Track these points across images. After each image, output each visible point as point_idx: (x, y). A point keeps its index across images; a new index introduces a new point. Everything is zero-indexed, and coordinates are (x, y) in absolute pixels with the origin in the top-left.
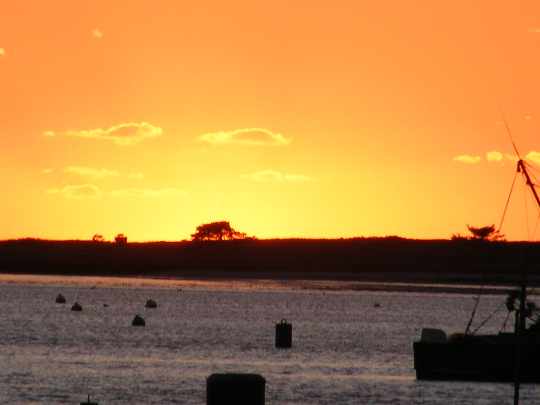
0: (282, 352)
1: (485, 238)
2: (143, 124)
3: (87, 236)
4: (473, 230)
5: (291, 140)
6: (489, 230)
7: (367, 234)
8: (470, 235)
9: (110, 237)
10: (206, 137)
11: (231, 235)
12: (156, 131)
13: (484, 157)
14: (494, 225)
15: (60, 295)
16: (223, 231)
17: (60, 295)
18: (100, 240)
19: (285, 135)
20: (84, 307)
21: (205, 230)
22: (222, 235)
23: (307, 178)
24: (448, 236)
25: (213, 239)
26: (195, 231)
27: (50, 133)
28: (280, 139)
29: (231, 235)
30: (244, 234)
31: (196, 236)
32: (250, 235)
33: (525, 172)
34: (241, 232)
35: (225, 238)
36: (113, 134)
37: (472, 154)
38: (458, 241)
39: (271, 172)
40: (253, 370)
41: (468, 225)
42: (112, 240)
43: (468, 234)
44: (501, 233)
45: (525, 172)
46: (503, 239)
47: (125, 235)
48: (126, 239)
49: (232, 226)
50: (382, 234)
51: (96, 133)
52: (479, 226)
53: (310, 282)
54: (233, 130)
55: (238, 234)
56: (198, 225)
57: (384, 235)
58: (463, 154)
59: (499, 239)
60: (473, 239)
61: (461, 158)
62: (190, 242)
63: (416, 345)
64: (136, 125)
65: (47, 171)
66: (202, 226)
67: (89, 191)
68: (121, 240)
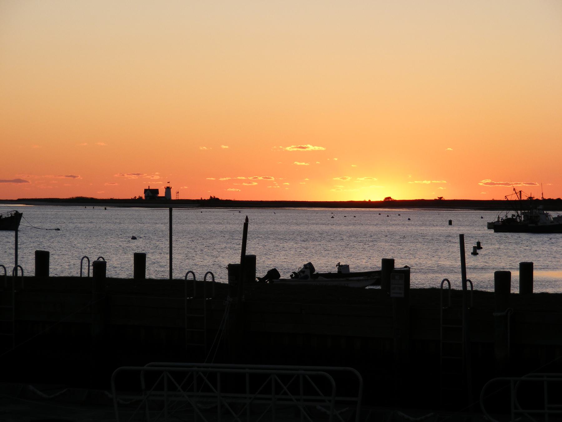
0: (450, 226)
6: (442, 198)
7: (418, 199)
8: (438, 199)
9: (367, 200)
10: (358, 179)
12: (349, 178)
14: (201, 198)
15: (488, 223)
17: (488, 223)
21: (386, 198)
24: (433, 199)
28: (375, 179)
33: (515, 191)
35: (390, 200)
36: (365, 179)
38: (435, 200)
40: (556, 236)
45: (515, 191)
51: (338, 179)
53: (415, 209)
57: (414, 199)
62: (367, 202)
63: (244, 223)
65: (145, 183)
66: (71, 198)
68: (370, 201)
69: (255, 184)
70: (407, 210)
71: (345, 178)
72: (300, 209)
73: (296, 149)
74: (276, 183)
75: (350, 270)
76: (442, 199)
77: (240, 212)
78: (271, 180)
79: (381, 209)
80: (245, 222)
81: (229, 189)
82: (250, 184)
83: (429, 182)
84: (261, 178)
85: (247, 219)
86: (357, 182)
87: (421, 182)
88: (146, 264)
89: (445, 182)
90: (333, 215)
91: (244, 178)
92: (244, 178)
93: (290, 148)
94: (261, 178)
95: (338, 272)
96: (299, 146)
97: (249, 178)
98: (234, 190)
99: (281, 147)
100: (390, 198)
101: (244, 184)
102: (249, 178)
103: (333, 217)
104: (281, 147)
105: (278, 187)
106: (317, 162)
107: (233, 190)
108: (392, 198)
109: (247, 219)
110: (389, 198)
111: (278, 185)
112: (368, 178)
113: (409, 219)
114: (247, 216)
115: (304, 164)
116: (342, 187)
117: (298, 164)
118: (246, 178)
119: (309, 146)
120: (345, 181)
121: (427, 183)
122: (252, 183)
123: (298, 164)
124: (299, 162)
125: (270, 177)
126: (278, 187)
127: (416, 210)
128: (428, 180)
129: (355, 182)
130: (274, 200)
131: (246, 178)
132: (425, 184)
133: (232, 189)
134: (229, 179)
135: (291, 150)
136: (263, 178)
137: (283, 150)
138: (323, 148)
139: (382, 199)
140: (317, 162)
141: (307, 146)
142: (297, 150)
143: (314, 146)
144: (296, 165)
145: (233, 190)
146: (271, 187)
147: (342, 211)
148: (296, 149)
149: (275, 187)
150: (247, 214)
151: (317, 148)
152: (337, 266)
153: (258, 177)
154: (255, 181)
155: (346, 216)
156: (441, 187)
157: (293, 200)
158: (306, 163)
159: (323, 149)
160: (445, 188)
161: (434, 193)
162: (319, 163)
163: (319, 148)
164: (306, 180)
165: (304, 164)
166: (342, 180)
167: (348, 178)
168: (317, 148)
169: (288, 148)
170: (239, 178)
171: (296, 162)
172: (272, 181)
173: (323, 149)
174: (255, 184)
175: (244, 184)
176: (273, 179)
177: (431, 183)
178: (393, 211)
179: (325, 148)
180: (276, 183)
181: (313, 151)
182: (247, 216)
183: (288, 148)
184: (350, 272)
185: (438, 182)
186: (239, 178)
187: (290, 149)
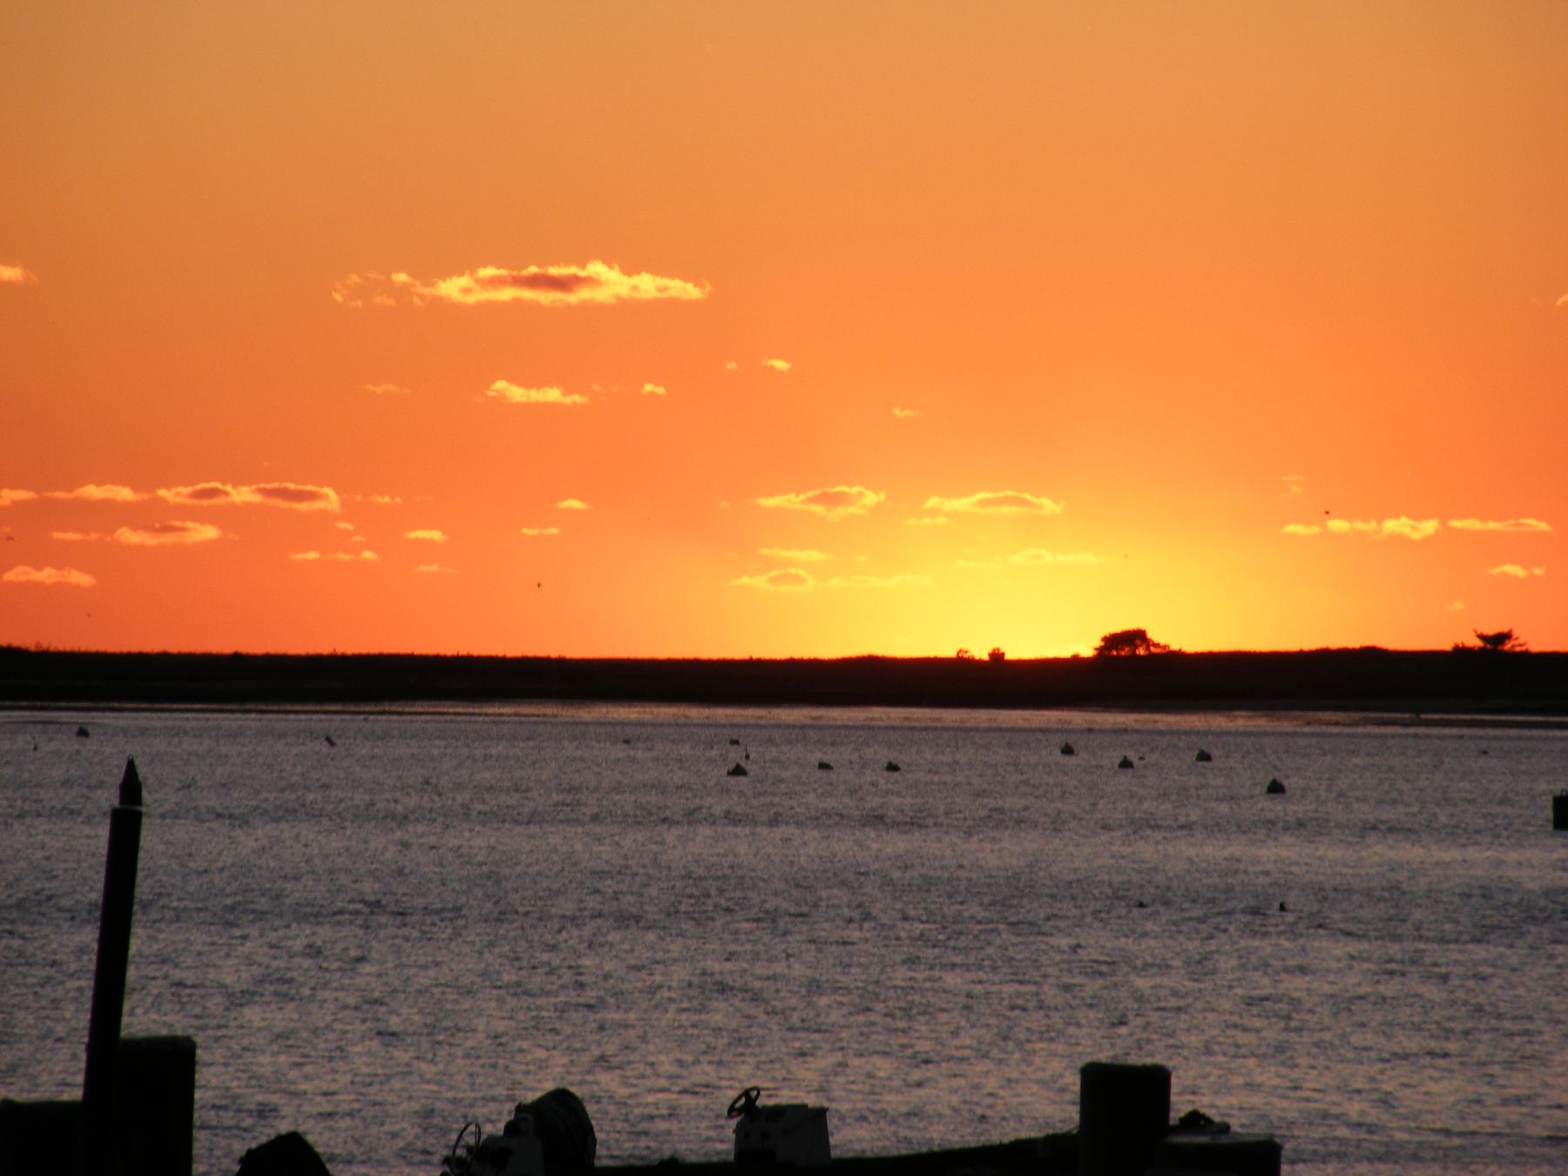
1: (1500, 648)
2: (856, 489)
3: (948, 651)
4: (1482, 637)
5: (1063, 504)
6: (1504, 637)
7: (1335, 641)
8: (1478, 643)
9: (981, 653)
10: (933, 502)
11: (1148, 648)
12: (871, 498)
13: (1323, 526)
15: (1125, 758)
16: (1138, 642)
17: (1125, 758)
18: (966, 656)
19: (1055, 500)
20: (1286, 783)
22: (1136, 647)
23: (1087, 558)
24: (1446, 645)
25: (1123, 653)
26: (1098, 643)
27: (725, 504)
28: (1048, 506)
29: (1148, 648)
30: (1165, 647)
31: (1100, 650)
32: (1174, 647)
34: (1162, 643)
35: (1141, 651)
36: (985, 503)
37: (1307, 522)
38: (1461, 652)
39: (1033, 551)
41: (1475, 631)
42: (986, 657)
43: (1475, 643)
44: (1521, 641)
46: (1524, 648)
47: (1002, 649)
48: (1003, 654)
49: (1150, 635)
50: (1354, 641)
52: (1491, 631)
53: (1311, 715)
54: (804, 491)
55: (1157, 645)
56: (1103, 635)
58: (1290, 522)
59: (1518, 649)
60: (1481, 649)
61: (1291, 528)
62: (980, 662)
64: (318, 489)
67: (797, 579)
68: (997, 656)
69: (209, 533)
70: (1261, 723)
71: (840, 499)
72: (507, 710)
73: (507, 294)
74: (349, 527)
75: (832, 1141)
76: (1508, 646)
77: (83, 733)
78: (319, 505)
79: (1077, 718)
80: (116, 802)
81: (19, 569)
82: (169, 538)
83: (1429, 527)
84: (243, 495)
85: (131, 787)
86: (926, 521)
87: (1373, 525)
88: (197, 1095)
89: (1543, 526)
90: (735, 756)
91: (125, 494)
92: (125, 494)
93: (464, 281)
94: (243, 495)
95: (741, 1151)
96: (533, 269)
97: (162, 492)
98: (49, 581)
99: (401, 277)
100: (1137, 637)
101: (127, 536)
102: (162, 492)
103: (738, 771)
104: (401, 277)
105: (368, 555)
106: (648, 388)
107: (47, 575)
108: (1155, 635)
109: (131, 787)
110: (1136, 637)
111: (368, 547)
112: (1000, 494)
113: (1276, 788)
114: (131, 768)
115: (553, 394)
116: (815, 555)
117: (517, 394)
118: (144, 496)
119: (596, 269)
120: (841, 511)
121: (1416, 536)
122: (183, 529)
123: (517, 394)
124: (526, 383)
125: (310, 488)
126: (368, 555)
127: (1320, 722)
128: (1418, 516)
129: (912, 522)
130: (554, 654)
131: (144, 496)
132: (1398, 540)
133: (39, 568)
134: (17, 504)
135: (471, 299)
136: (261, 491)
137: (416, 300)
138: (690, 287)
139: (1086, 648)
140: (648, 388)
141: (581, 273)
142: (517, 302)
143: (628, 270)
144: (501, 398)
145: (47, 575)
146: (313, 555)
147: (803, 727)
148: (507, 294)
149: (342, 556)
150: (133, 748)
151: (647, 285)
152: (732, 1110)
153: (229, 488)
154: (204, 517)
155: (826, 759)
156: (1514, 563)
157: (463, 652)
158: (567, 392)
159: (692, 292)
160: (1537, 571)
161: (1459, 605)
162: (661, 390)
163: (661, 289)
164: (571, 511)
165: (553, 394)
166: (819, 509)
167: (860, 495)
168: (647, 285)
169: (452, 288)
170: (92, 491)
171: (501, 385)
172: (323, 513)
173: (692, 292)
174: (209, 533)
175: (127, 536)
176: (331, 499)
177: (1446, 534)
178: (1161, 727)
179: (709, 287)
180: (349, 527)
181: (626, 308)
182: (131, 768)
183: (452, 288)
184: (835, 1153)
185: (1492, 525)
186: (92, 491)
187: (467, 291)
